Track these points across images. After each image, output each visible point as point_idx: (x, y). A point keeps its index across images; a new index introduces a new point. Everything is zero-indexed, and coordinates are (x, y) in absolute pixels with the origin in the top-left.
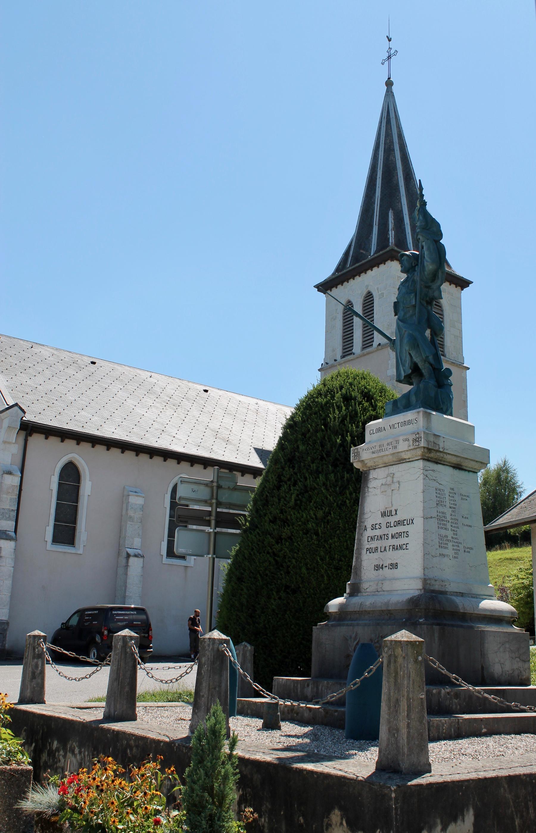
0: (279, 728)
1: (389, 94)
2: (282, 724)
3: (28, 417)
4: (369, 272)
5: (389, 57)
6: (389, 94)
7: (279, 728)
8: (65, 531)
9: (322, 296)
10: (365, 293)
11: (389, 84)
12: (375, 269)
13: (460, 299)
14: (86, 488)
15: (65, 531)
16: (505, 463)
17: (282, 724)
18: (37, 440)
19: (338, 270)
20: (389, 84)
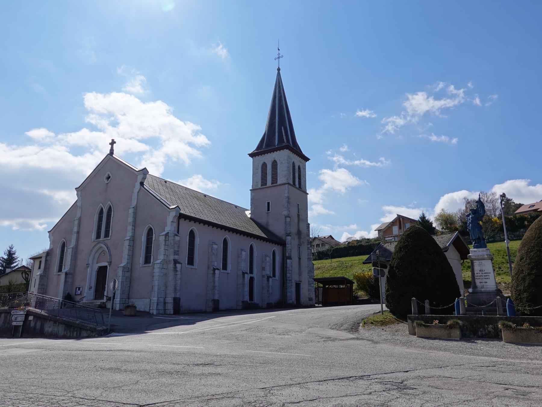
0: (485, 247)
1: (279, 74)
2: (487, 244)
3: (182, 212)
4: (275, 152)
5: (279, 58)
6: (279, 74)
7: (485, 247)
8: (191, 261)
9: (251, 159)
10: (273, 160)
11: (279, 70)
12: (278, 151)
13: (305, 165)
14: (197, 241)
15: (191, 261)
16: (398, 215)
17: (487, 244)
18: (182, 221)
19: (258, 148)
20: (279, 70)
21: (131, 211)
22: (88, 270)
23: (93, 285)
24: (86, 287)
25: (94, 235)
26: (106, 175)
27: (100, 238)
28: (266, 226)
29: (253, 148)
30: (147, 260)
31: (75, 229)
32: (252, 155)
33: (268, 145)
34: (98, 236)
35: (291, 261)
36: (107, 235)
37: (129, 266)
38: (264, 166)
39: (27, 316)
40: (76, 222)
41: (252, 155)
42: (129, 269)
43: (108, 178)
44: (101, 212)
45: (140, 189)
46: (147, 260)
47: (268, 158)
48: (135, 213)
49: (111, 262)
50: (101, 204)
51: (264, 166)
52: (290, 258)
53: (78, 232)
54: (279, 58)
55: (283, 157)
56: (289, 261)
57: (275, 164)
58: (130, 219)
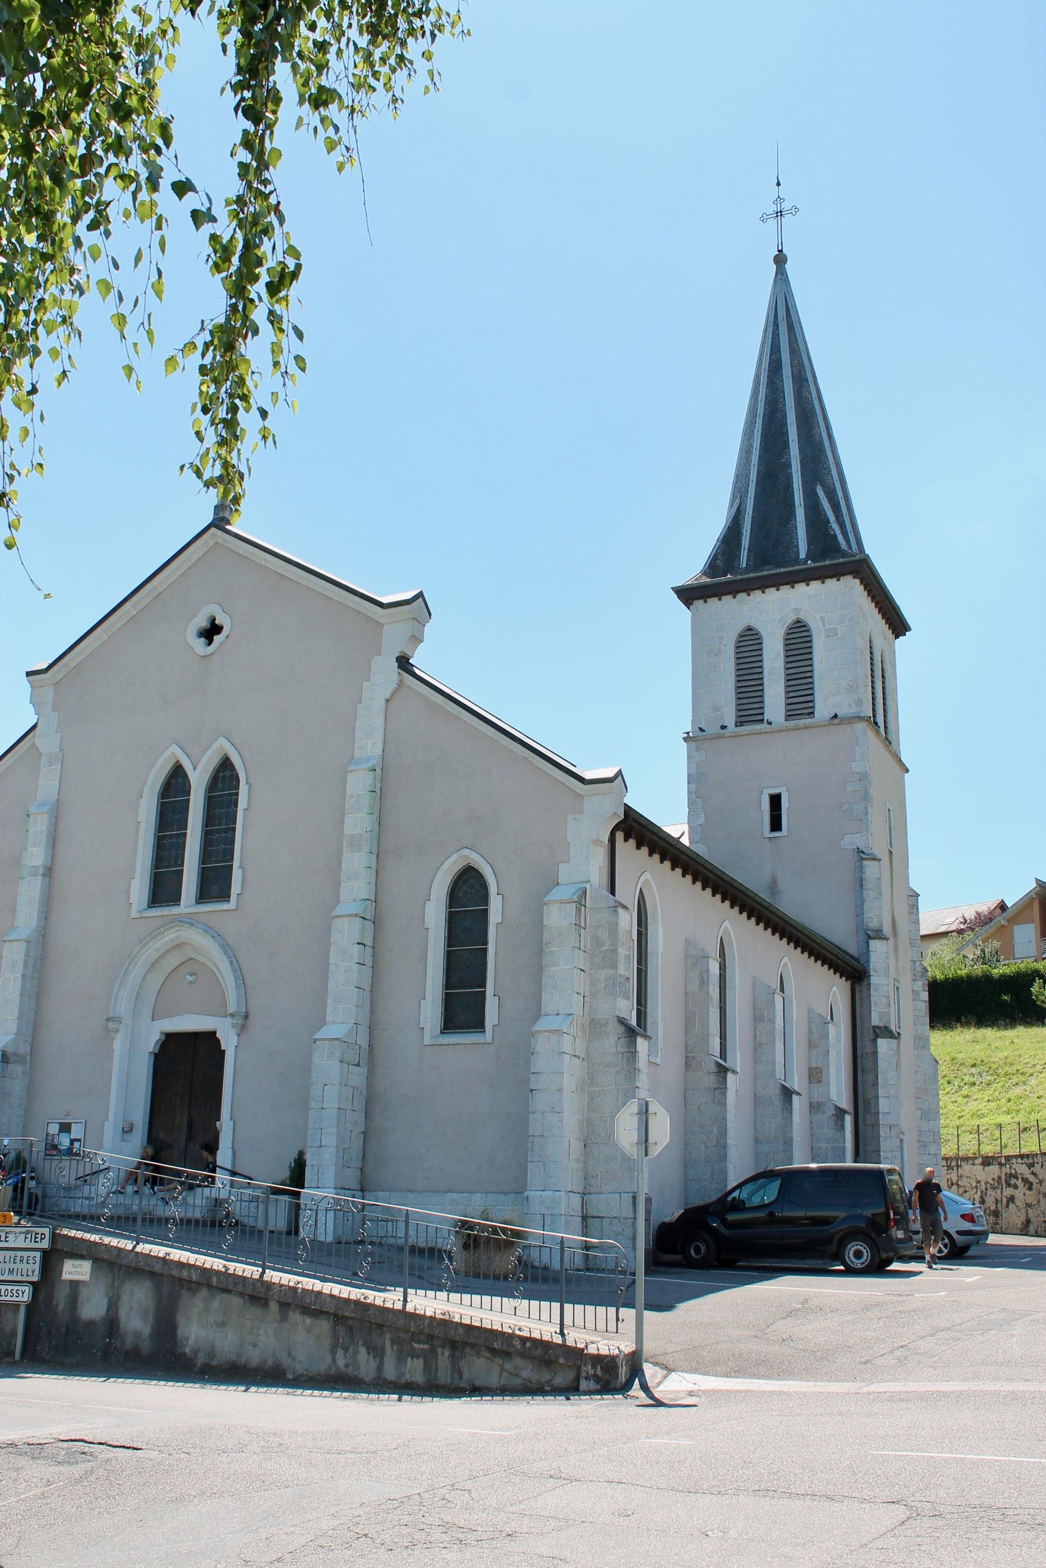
1: (781, 274)
5: (780, 214)
6: (781, 274)
10: (791, 619)
11: (780, 260)
19: (712, 568)
20: (780, 260)
21: (359, 783)
22: (117, 1044)
23: (140, 1115)
24: (109, 1126)
25: (140, 887)
26: (203, 623)
27: (175, 899)
28: (764, 895)
29: (692, 568)
30: (463, 1010)
31: (36, 856)
32: (688, 595)
33: (761, 556)
34: (163, 890)
35: (893, 1043)
36: (215, 884)
37: (363, 1041)
38: (749, 643)
39: (51, 1260)
40: (39, 826)
41: (688, 595)
42: (370, 1054)
43: (211, 631)
44: (176, 782)
45: (400, 683)
46: (463, 1010)
47: (770, 610)
48: (381, 794)
49: (246, 1016)
50: (175, 749)
51: (749, 643)
52: (886, 1032)
53: (49, 872)
54: (780, 214)
55: (826, 605)
56: (883, 1045)
57: (799, 639)
58: (358, 822)
